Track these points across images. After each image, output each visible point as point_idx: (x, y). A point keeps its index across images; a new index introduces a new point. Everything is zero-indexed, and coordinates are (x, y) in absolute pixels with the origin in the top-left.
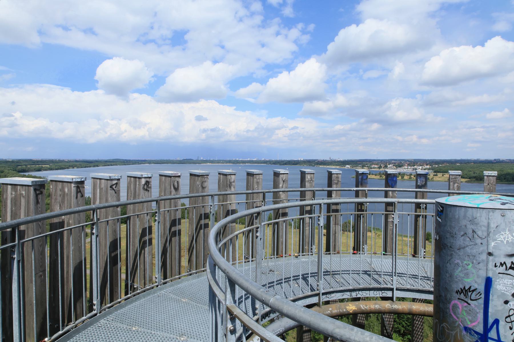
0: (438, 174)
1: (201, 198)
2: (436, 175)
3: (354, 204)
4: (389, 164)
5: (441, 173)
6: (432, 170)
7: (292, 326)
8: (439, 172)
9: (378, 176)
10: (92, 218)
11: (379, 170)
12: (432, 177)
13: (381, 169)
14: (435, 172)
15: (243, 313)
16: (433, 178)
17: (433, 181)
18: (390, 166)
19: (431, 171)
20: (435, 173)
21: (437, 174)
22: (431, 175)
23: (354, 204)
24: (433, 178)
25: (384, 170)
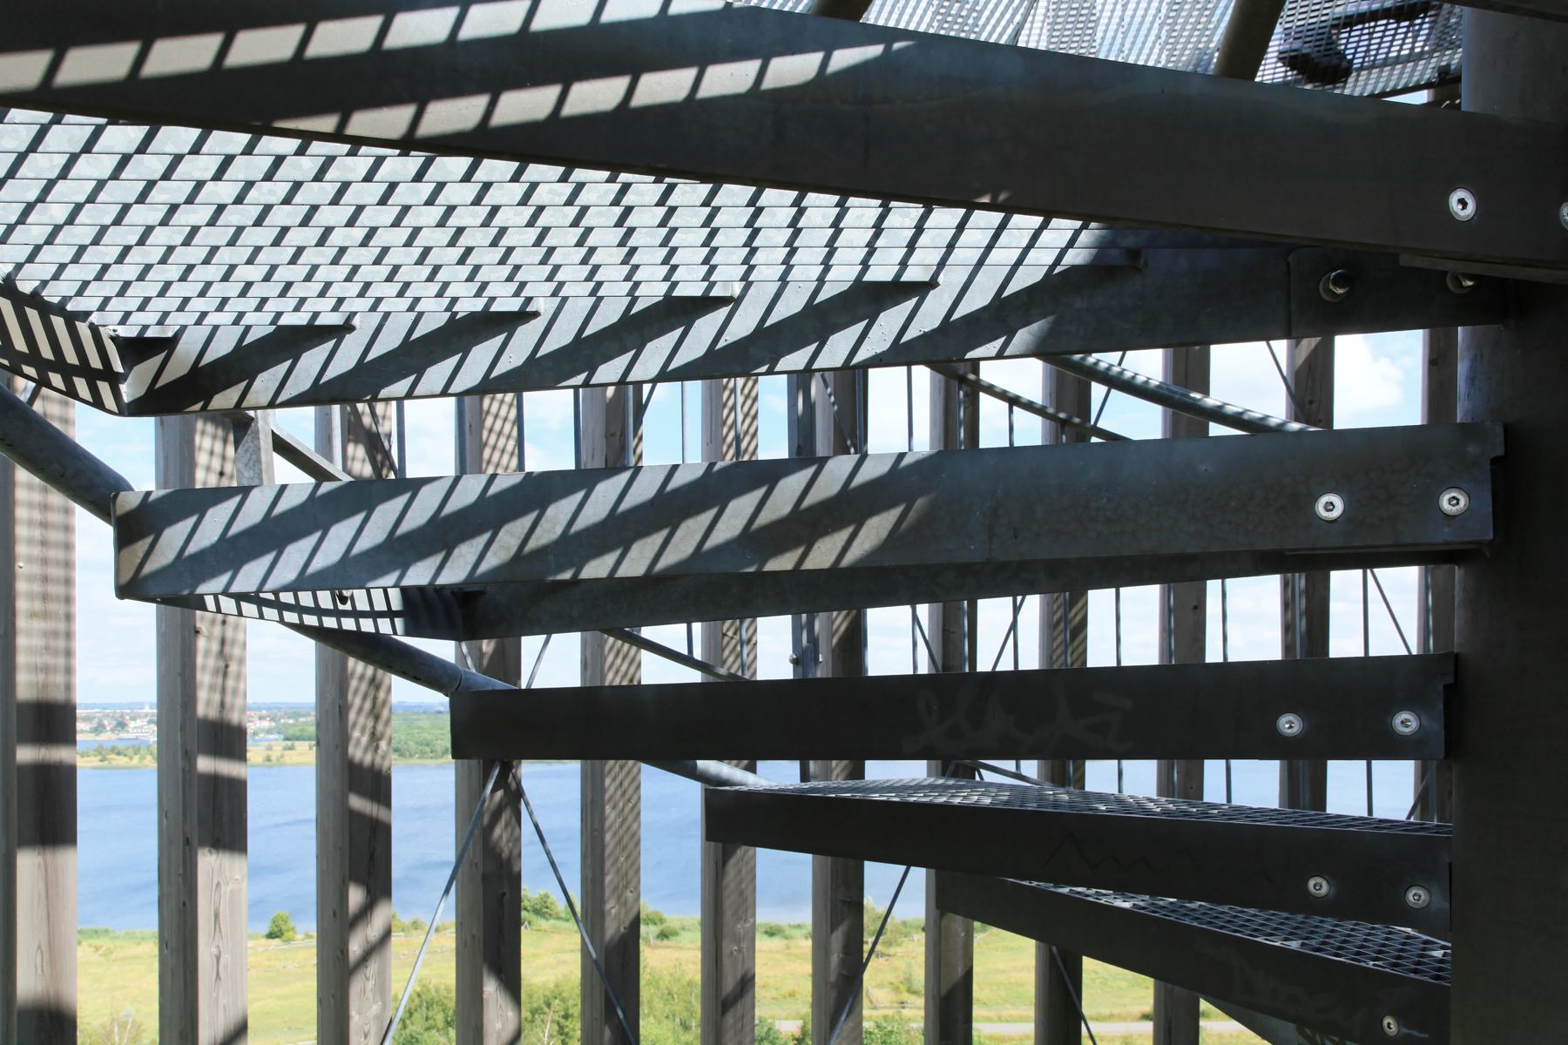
0: (297, 743)
1: (394, 403)
2: (291, 748)
3: (572, 391)
4: (134, 719)
5: (304, 739)
6: (279, 733)
7: (232, 1028)
8: (298, 739)
9: (92, 758)
10: (20, 344)
11: (98, 738)
12: (279, 754)
13: (103, 737)
14: (287, 739)
15: (302, 562)
16: (282, 757)
17: (282, 765)
18: (138, 723)
19: (276, 736)
20: (289, 743)
21: (293, 745)
22: (274, 748)
23: (572, 391)
24: (282, 757)
25: (113, 737)
